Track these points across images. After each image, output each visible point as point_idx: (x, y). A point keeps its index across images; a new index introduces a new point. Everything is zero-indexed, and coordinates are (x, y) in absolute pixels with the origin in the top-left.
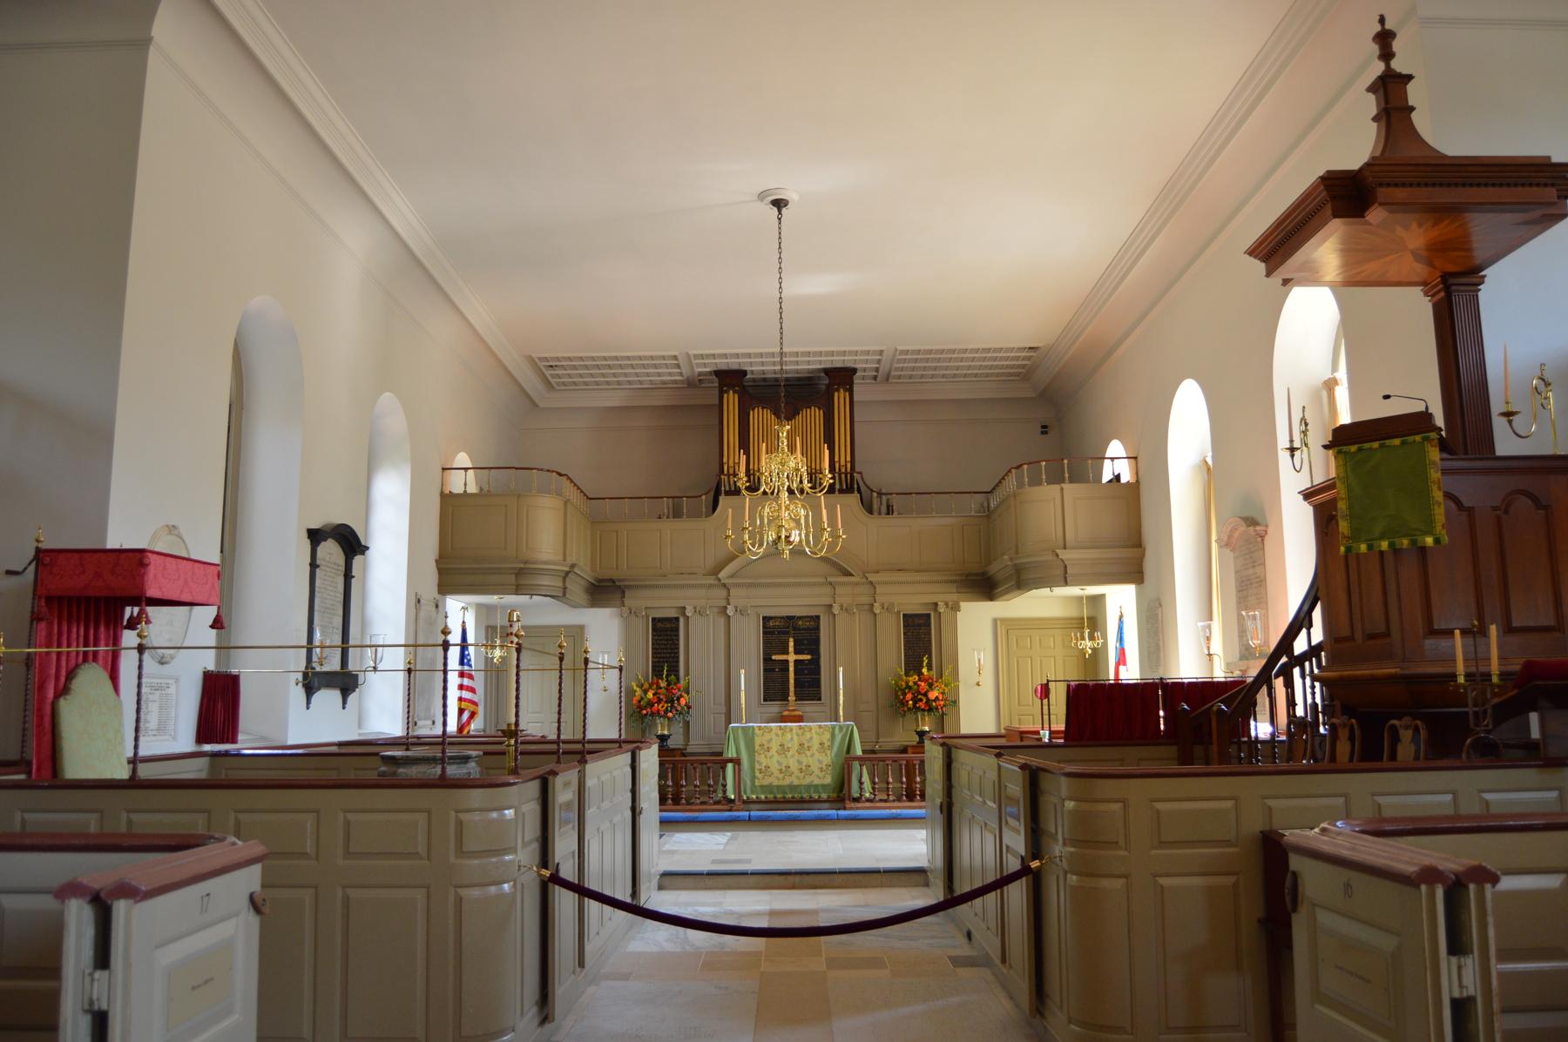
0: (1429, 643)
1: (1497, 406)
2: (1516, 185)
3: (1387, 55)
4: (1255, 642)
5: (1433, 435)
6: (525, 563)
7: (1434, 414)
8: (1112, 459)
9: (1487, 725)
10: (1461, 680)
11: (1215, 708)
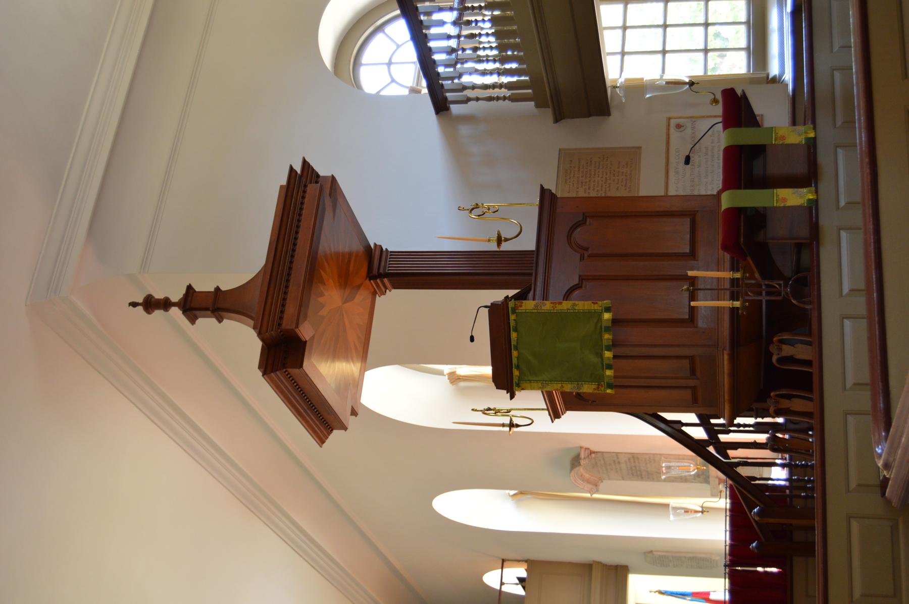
0: (701, 323)
1: (493, 247)
2: (300, 215)
3: (166, 304)
4: (692, 469)
5: (511, 304)
7: (492, 301)
8: (502, 584)
9: (780, 285)
10: (737, 304)
11: (757, 518)
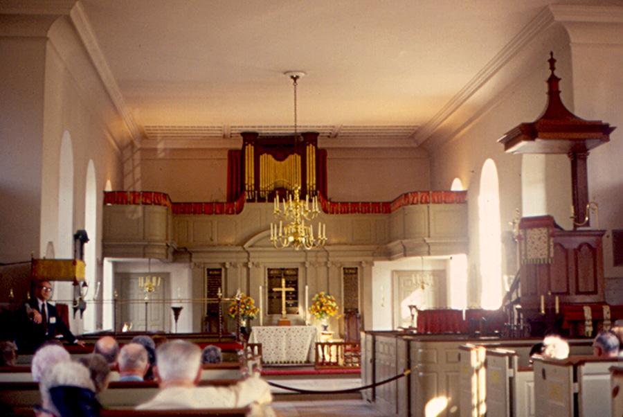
3: (552, 68)
6: (149, 242)
